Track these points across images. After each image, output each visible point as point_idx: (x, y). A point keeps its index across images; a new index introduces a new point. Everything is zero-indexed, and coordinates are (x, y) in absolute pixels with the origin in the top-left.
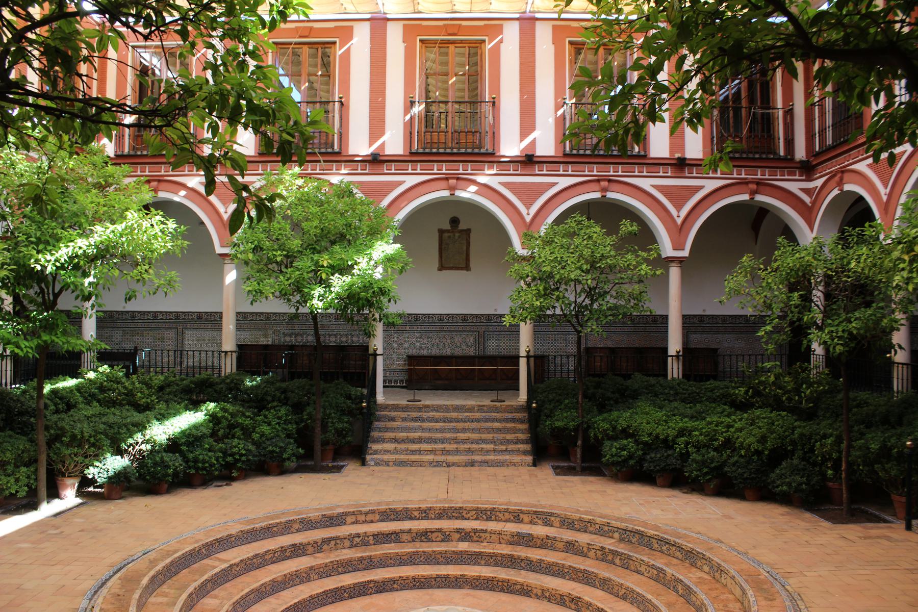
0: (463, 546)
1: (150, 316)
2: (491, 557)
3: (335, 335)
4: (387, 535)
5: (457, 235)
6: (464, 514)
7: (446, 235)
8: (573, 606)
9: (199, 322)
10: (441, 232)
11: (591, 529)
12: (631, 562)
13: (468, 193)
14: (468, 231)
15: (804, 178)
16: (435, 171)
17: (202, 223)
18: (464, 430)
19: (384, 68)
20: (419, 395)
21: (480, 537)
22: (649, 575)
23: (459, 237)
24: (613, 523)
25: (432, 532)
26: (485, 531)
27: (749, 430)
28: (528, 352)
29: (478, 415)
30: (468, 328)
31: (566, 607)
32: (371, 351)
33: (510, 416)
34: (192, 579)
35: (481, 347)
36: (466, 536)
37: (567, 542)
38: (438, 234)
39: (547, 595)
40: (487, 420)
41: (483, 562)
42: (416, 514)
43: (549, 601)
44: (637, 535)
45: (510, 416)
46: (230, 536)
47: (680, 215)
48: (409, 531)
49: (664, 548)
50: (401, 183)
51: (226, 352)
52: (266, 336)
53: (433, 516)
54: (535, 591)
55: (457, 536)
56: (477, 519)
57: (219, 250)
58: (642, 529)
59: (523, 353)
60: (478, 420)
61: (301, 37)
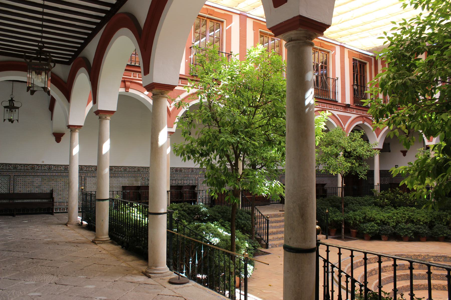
1: (62, 168)
19: (377, 66)
24: (430, 255)
27: (422, 215)
39: (436, 287)
43: (437, 290)
52: (137, 181)
61: (209, 14)
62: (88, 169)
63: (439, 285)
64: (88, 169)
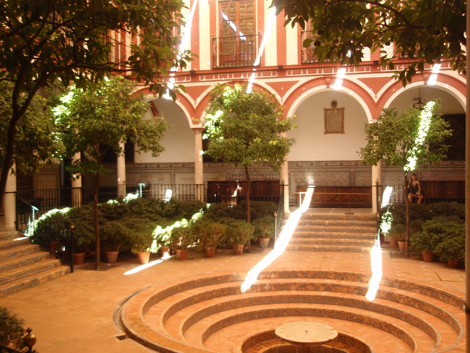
0: (324, 294)
2: (342, 300)
3: (263, 175)
4: (282, 286)
5: (336, 112)
6: (328, 276)
7: (329, 112)
8: (387, 330)
9: (183, 168)
10: (326, 110)
11: (403, 287)
12: (424, 306)
13: (337, 86)
14: (343, 109)
15: (276, 76)
16: (317, 74)
17: (182, 111)
18: (336, 231)
20: (352, 210)
21: (336, 289)
22: (434, 314)
23: (337, 113)
25: (308, 285)
26: (339, 286)
28: (377, 183)
29: (345, 222)
30: (344, 170)
31: (383, 330)
32: (281, 183)
33: (366, 222)
34: (166, 305)
35: (352, 181)
36: (328, 288)
37: (387, 294)
38: (323, 112)
40: (351, 225)
41: (337, 303)
42: (300, 275)
43: (374, 326)
44: (430, 291)
45: (366, 222)
46: (194, 282)
47: (376, 98)
48: (295, 284)
49: (445, 299)
50: (296, 82)
51: (197, 185)
53: (310, 276)
54: (365, 320)
55: (323, 288)
56: (335, 279)
57: (192, 126)
58: (433, 287)
59: (374, 183)
60: (345, 225)
62: (318, 164)
63: (376, 321)
64: (176, 166)
